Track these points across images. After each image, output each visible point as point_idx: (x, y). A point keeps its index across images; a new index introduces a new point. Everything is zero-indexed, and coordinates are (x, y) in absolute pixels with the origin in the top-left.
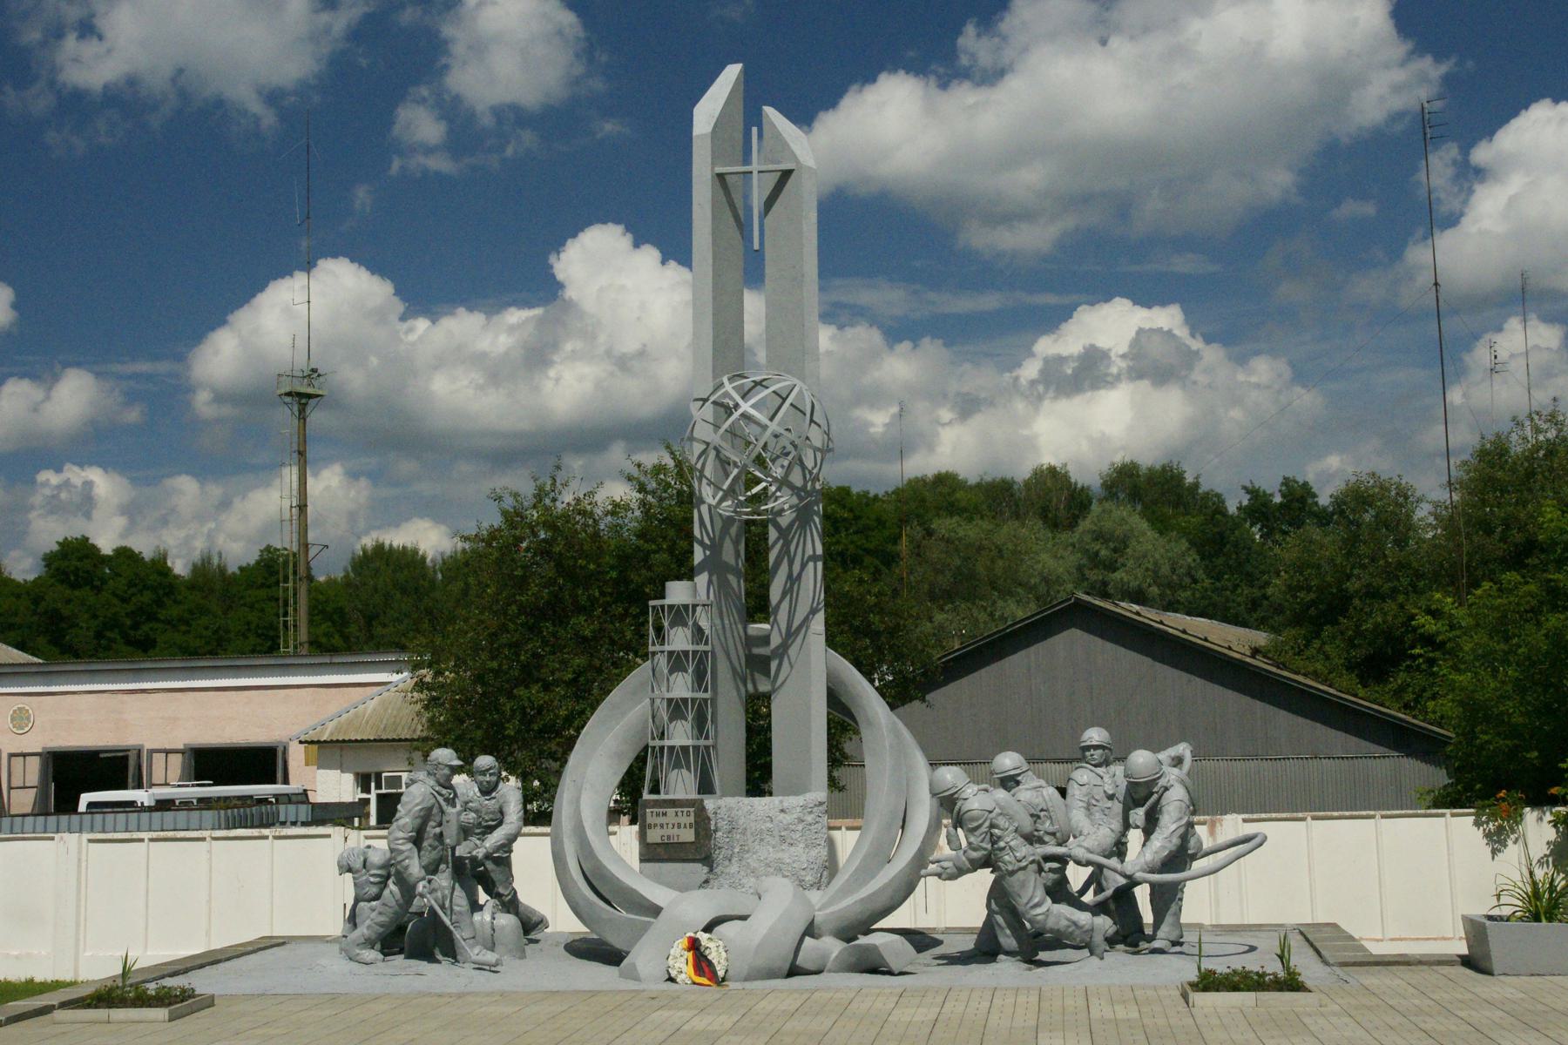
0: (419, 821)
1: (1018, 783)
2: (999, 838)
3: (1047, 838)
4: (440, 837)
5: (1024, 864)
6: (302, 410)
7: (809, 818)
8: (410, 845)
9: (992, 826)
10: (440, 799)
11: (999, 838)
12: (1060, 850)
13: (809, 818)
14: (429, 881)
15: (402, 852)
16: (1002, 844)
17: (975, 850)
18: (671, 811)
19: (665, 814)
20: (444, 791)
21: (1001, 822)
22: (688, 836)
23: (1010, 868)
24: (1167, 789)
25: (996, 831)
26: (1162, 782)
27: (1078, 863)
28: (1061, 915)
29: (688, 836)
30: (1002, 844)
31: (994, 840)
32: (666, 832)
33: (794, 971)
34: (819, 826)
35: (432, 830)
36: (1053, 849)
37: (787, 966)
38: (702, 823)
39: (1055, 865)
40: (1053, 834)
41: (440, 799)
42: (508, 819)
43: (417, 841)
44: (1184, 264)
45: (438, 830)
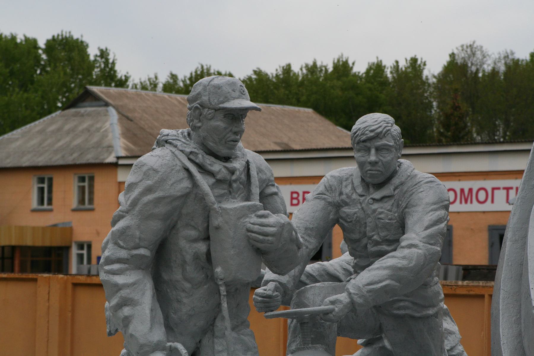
10: (204, 183)
15: (118, 288)
20: (217, 166)
35: (188, 246)
41: (204, 183)
43: (159, 261)
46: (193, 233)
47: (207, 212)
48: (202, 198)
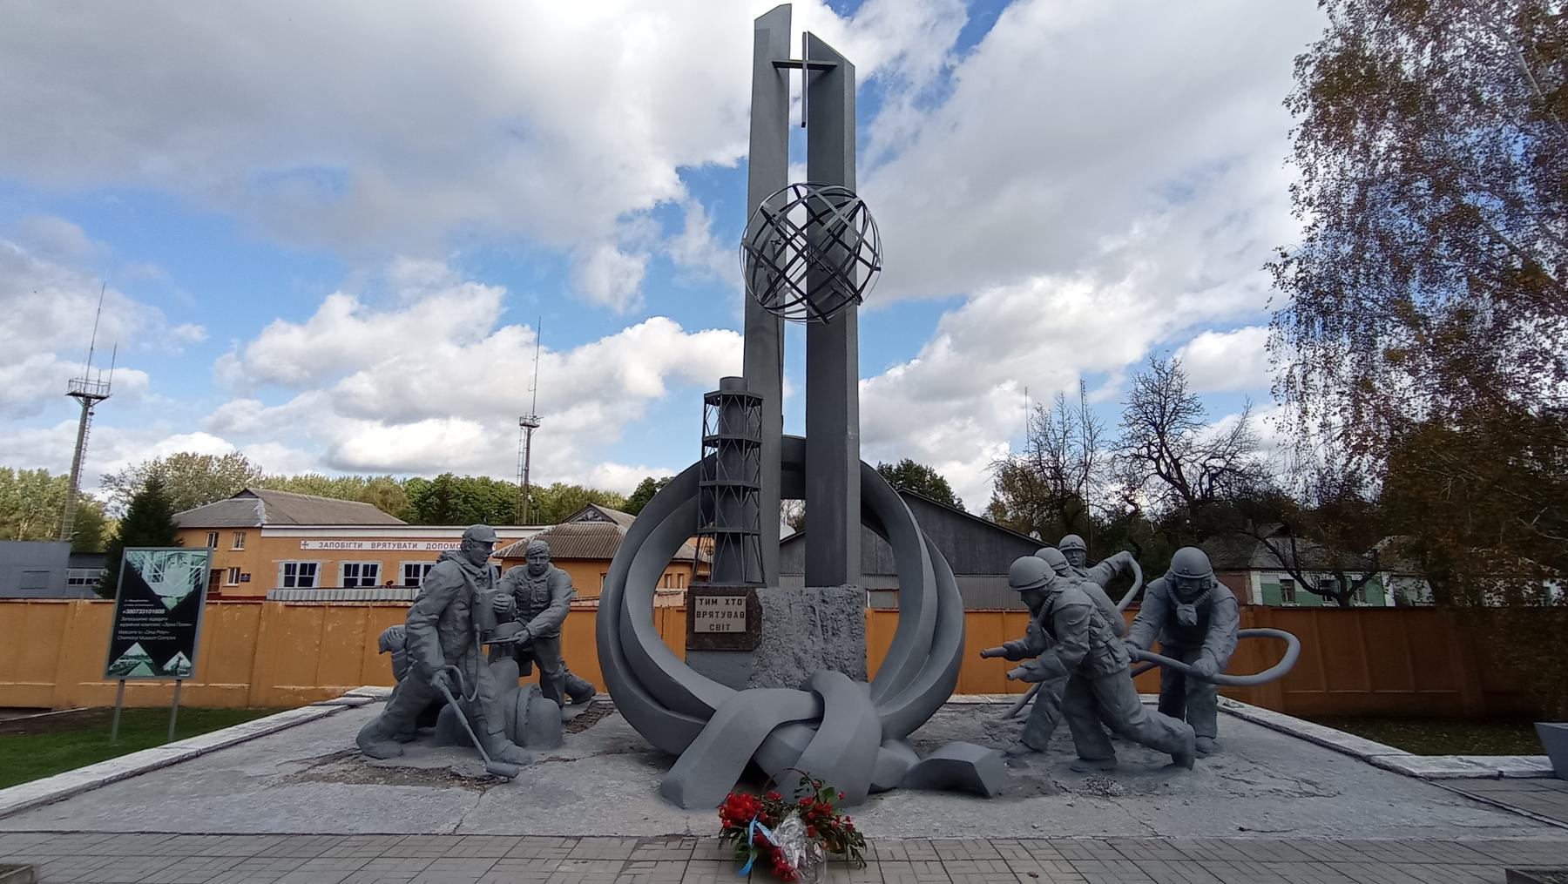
0: (444, 602)
8: (431, 630)
10: (471, 578)
14: (451, 673)
20: (477, 571)
21: (1100, 619)
22: (739, 625)
29: (739, 625)
31: (1093, 637)
38: (754, 614)
42: (556, 601)
47: (473, 596)
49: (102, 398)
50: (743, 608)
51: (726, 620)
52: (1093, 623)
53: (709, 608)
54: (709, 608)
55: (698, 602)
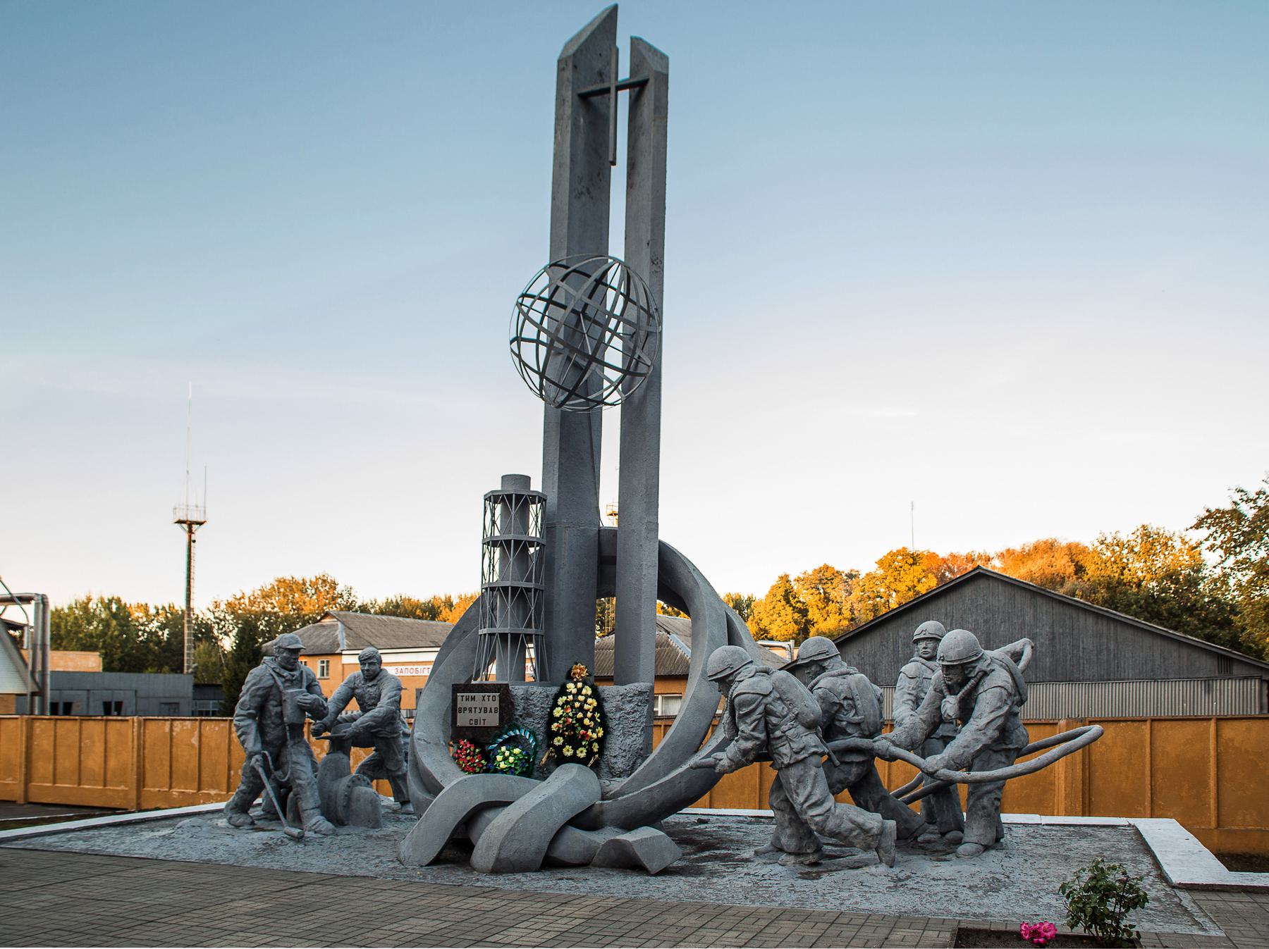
1: (824, 669)
2: (776, 726)
3: (849, 730)
4: (281, 715)
5: (801, 757)
6: (190, 532)
7: (628, 707)
9: (767, 712)
11: (776, 726)
12: (865, 742)
13: (628, 707)
16: (778, 733)
17: (746, 739)
18: (478, 695)
19: (473, 699)
20: (286, 674)
21: (779, 708)
22: (493, 720)
23: (786, 761)
24: (985, 674)
25: (774, 720)
26: (981, 666)
27: (882, 757)
28: (847, 812)
29: (493, 720)
30: (778, 733)
32: (473, 716)
33: (550, 863)
34: (637, 715)
35: (273, 709)
36: (855, 740)
37: (540, 859)
39: (859, 758)
40: (858, 724)
41: (279, 681)
44: (989, 787)
45: (279, 709)
46: (274, 703)
48: (278, 687)
49: (201, 524)
50: (496, 704)
51: (483, 715)
52: (767, 712)
53: (470, 704)
54: (470, 704)
55: (459, 699)
